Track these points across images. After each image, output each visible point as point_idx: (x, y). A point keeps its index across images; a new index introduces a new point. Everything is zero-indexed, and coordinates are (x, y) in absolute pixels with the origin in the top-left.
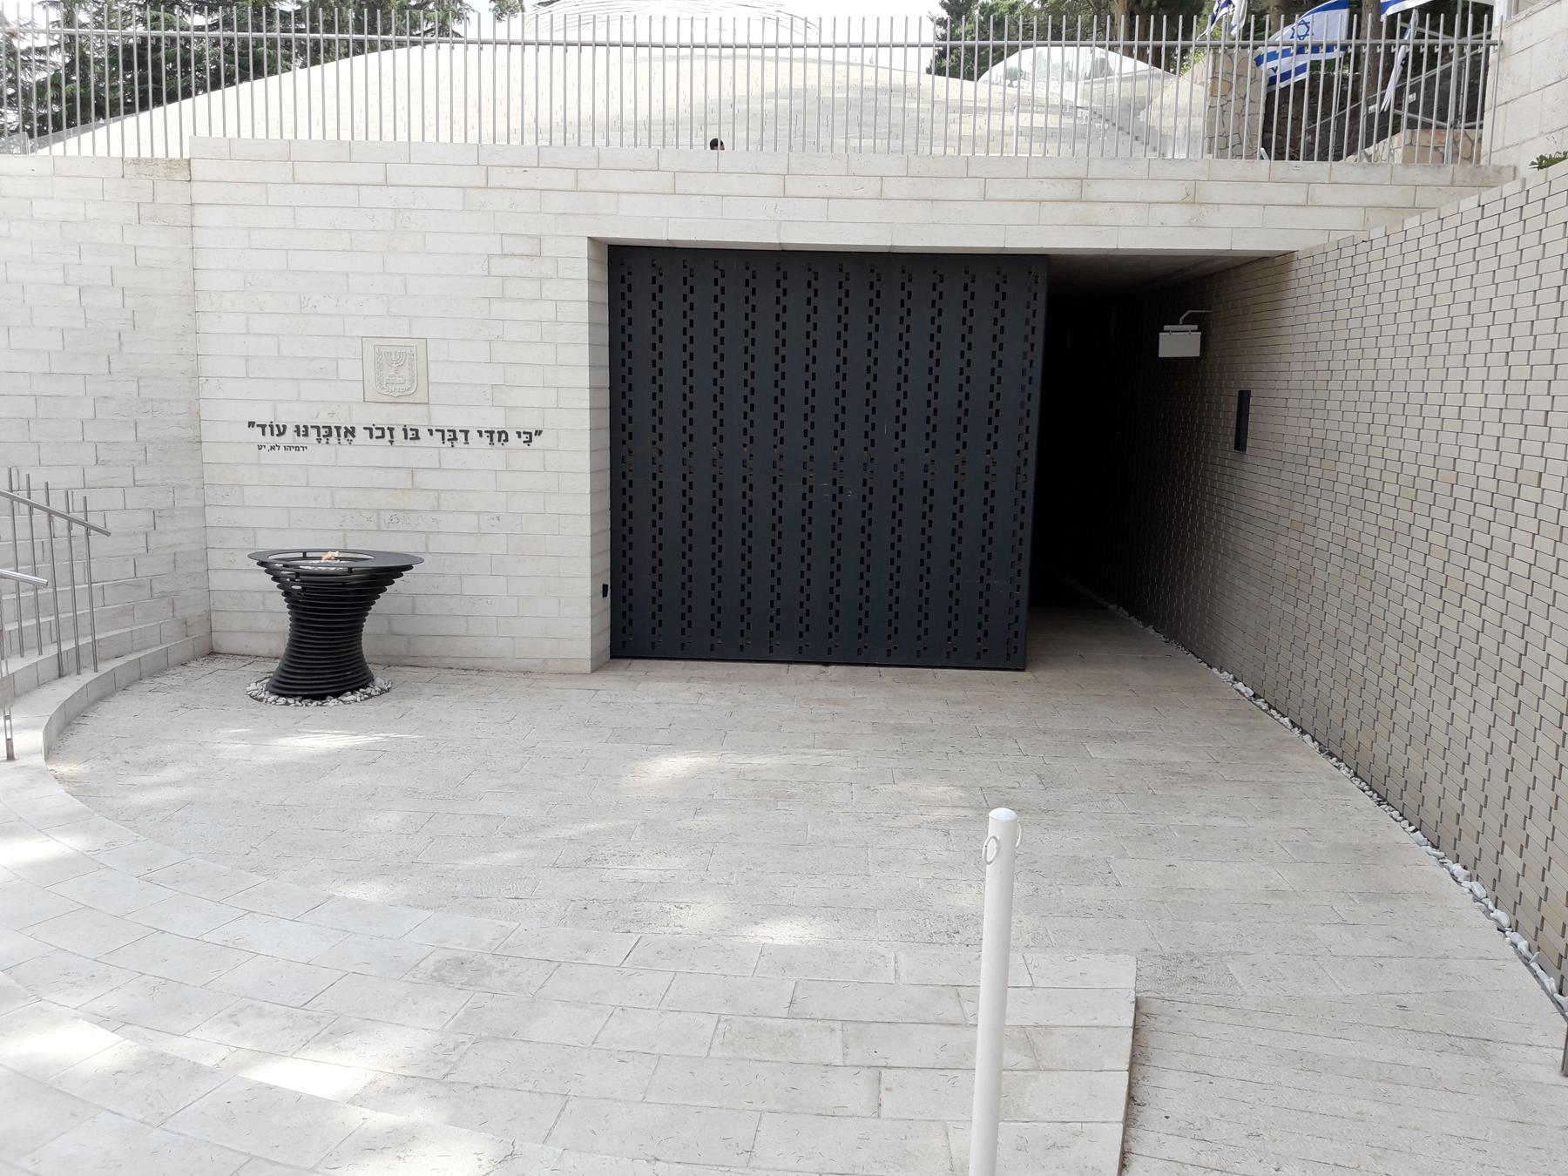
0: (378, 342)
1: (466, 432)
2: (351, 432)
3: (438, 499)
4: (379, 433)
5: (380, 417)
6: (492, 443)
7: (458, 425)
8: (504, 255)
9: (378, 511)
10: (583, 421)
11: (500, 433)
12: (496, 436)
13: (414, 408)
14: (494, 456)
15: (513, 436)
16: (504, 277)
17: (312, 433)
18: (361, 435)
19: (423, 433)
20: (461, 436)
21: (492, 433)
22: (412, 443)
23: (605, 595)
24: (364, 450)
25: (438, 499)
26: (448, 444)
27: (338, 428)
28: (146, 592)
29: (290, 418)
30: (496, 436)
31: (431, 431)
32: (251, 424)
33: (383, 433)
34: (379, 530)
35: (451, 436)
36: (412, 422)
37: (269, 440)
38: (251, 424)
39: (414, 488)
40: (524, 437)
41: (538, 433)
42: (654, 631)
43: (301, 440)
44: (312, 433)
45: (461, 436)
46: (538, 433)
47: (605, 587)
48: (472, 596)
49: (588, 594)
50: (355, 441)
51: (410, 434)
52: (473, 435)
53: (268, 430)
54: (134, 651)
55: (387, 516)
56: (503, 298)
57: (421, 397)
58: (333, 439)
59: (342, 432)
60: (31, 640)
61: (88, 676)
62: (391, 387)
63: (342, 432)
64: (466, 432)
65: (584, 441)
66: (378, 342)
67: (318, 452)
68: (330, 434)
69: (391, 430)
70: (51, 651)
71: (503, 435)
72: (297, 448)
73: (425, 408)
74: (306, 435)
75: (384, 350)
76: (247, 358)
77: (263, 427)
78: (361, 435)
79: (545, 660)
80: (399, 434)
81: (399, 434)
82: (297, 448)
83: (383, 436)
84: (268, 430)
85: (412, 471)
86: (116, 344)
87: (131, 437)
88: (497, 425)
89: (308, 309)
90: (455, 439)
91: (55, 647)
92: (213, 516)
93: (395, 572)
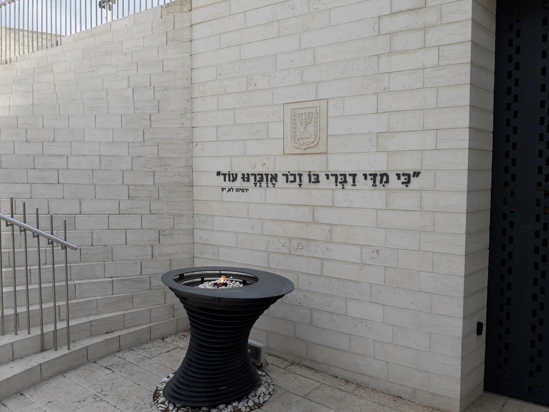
0: (294, 106)
1: (354, 176)
2: (274, 178)
3: (331, 232)
4: (291, 178)
5: (293, 165)
6: (374, 185)
7: (348, 169)
8: (393, 14)
9: (290, 239)
10: (462, 161)
11: (382, 176)
12: (378, 179)
13: (316, 157)
14: (374, 196)
15: (393, 178)
16: (391, 34)
17: (252, 178)
18: (281, 179)
19: (322, 177)
20: (350, 179)
21: (375, 175)
22: (313, 185)
23: (479, 332)
24: (284, 192)
25: (331, 232)
26: (340, 186)
27: (267, 175)
28: (147, 286)
29: (239, 169)
30: (378, 179)
31: (327, 176)
32: (218, 173)
33: (294, 178)
34: (290, 254)
35: (341, 179)
36: (314, 169)
37: (228, 184)
38: (218, 173)
39: (314, 222)
40: (403, 179)
41: (416, 174)
42: (531, 374)
43: (245, 185)
44: (252, 178)
45: (350, 179)
46: (416, 174)
47: (480, 325)
48: (354, 319)
49: (459, 334)
50: (277, 185)
51: (313, 178)
52: (360, 178)
53: (227, 177)
54: (125, 328)
55: (295, 243)
56: (391, 53)
57: (321, 148)
58: (264, 184)
59: (270, 177)
60: (23, 322)
61: (63, 351)
62: (301, 142)
63: (270, 177)
64: (354, 176)
65: (462, 181)
66: (294, 106)
67: (255, 193)
68: (262, 180)
69: (300, 175)
70: (36, 331)
71: (384, 178)
72: (243, 190)
73: (324, 157)
74: (248, 180)
75: (297, 112)
76: (217, 127)
77: (225, 175)
78: (281, 179)
79: (415, 390)
80: (305, 178)
81: (305, 178)
82: (243, 190)
83: (295, 181)
84: (227, 177)
85: (313, 208)
86: (148, 123)
87: (150, 182)
88: (380, 169)
89: (251, 88)
90: (345, 181)
91: (39, 328)
92: (198, 234)
93: (265, 303)
